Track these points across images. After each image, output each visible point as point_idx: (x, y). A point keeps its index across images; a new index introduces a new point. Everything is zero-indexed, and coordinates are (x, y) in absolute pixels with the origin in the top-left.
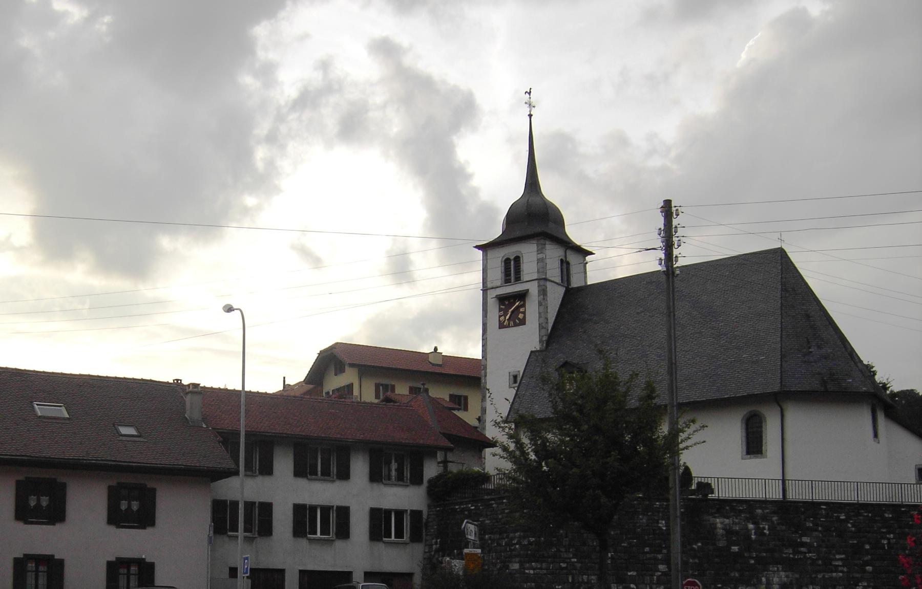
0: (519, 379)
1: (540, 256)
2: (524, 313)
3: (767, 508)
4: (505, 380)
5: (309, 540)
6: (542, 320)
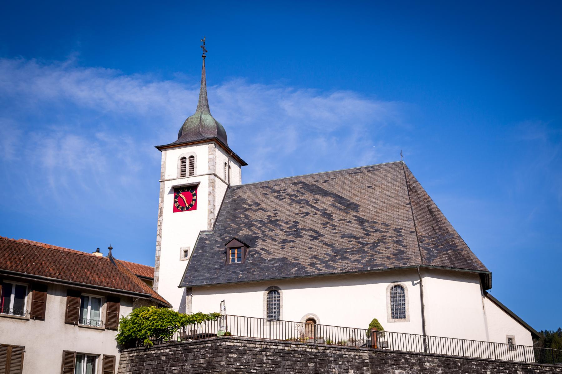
0: (189, 254)
1: (212, 156)
2: (195, 200)
3: (433, 362)
4: (178, 254)
5: (79, 327)
6: (211, 207)
